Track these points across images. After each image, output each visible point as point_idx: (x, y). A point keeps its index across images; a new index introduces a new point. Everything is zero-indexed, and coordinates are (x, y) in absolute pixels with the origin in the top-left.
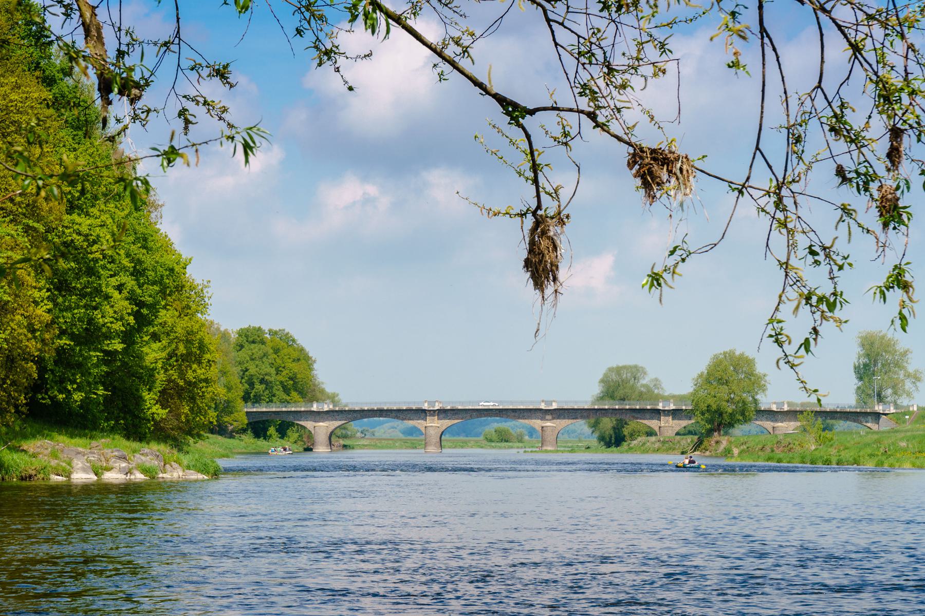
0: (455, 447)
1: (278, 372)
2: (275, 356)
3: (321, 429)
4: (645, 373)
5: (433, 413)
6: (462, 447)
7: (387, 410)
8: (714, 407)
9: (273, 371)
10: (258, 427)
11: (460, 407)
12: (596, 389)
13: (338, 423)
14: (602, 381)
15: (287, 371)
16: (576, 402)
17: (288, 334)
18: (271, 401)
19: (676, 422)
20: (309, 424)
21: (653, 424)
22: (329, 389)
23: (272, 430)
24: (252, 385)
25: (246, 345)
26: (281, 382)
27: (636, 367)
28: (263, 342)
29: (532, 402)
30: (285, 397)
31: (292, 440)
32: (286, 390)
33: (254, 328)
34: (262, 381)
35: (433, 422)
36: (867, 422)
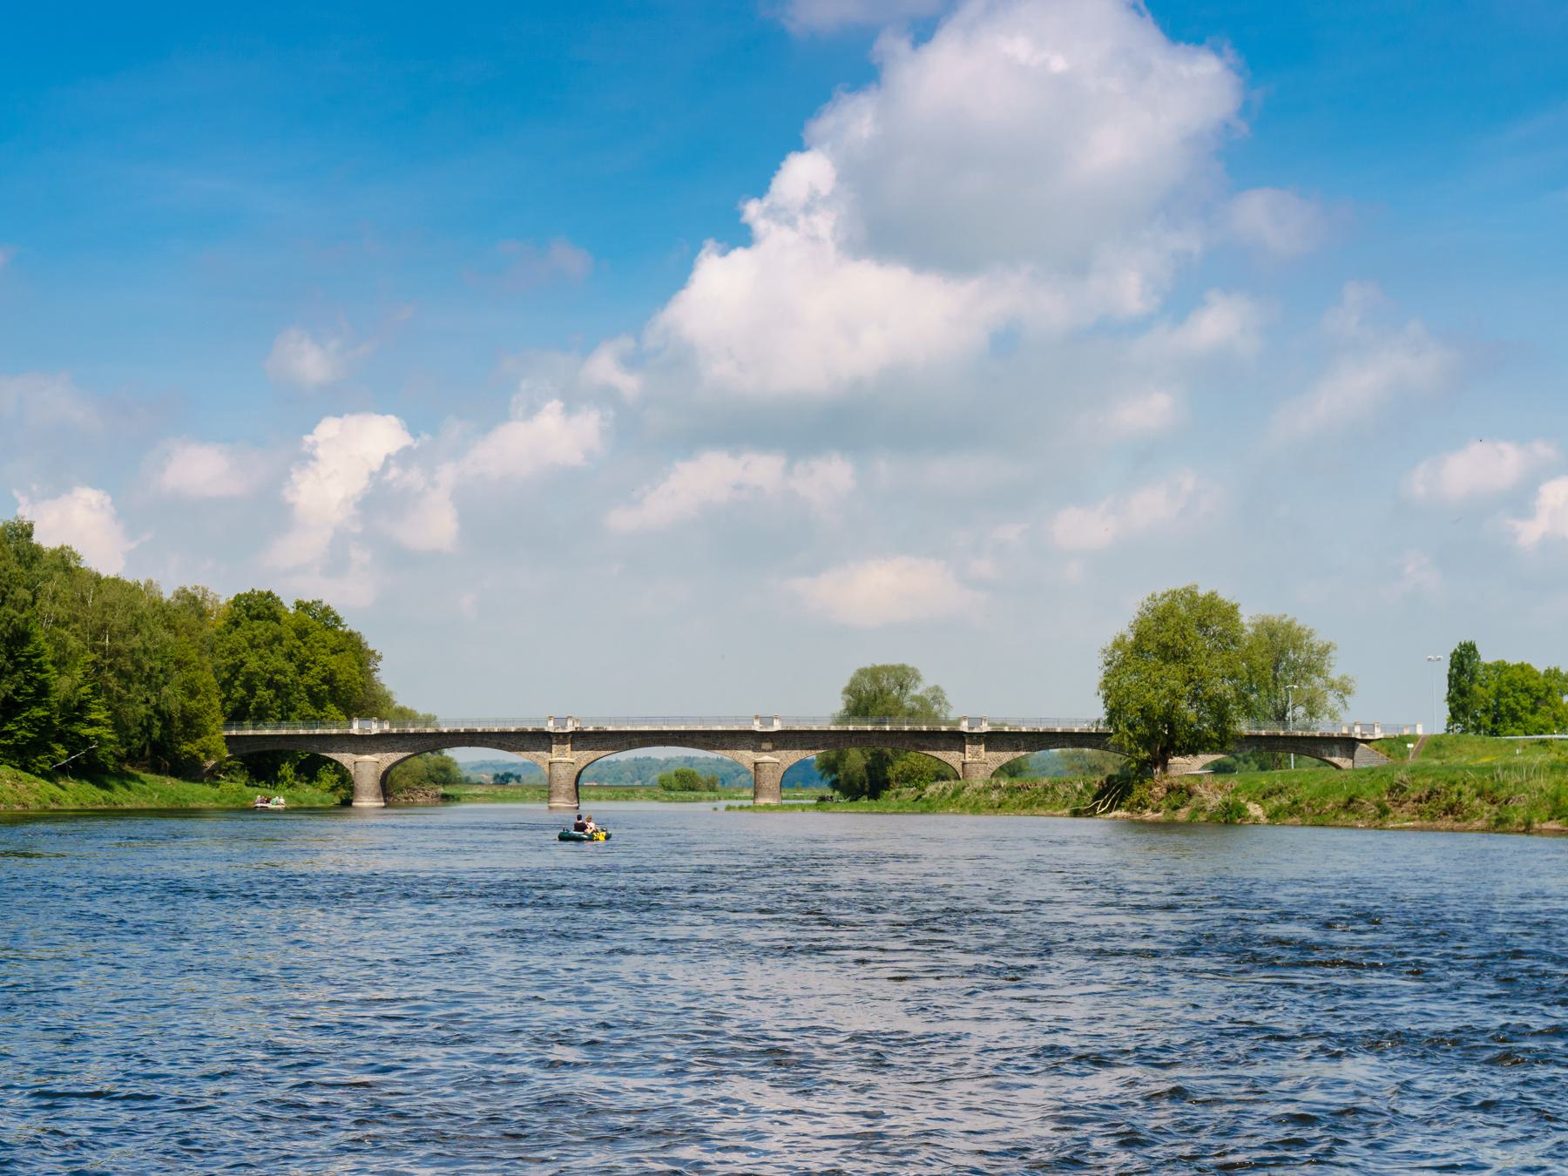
0: (616, 799)
1: (302, 669)
2: (298, 643)
3: (367, 766)
4: (918, 679)
5: (562, 738)
6: (627, 798)
7: (483, 734)
8: (1159, 709)
9: (291, 667)
10: (261, 764)
11: (610, 729)
12: (838, 705)
13: (395, 757)
14: (849, 691)
15: (319, 669)
16: (814, 720)
17: (328, 608)
18: (286, 718)
19: (992, 754)
20: (346, 759)
21: (952, 758)
22: (401, 700)
23: (287, 769)
24: (251, 690)
25: (245, 623)
26: (309, 689)
27: (903, 668)
28: (277, 620)
29: (737, 720)
30: (312, 712)
31: (325, 785)
32: (317, 701)
33: (261, 595)
34: (270, 684)
35: (563, 755)
36: (1331, 755)
